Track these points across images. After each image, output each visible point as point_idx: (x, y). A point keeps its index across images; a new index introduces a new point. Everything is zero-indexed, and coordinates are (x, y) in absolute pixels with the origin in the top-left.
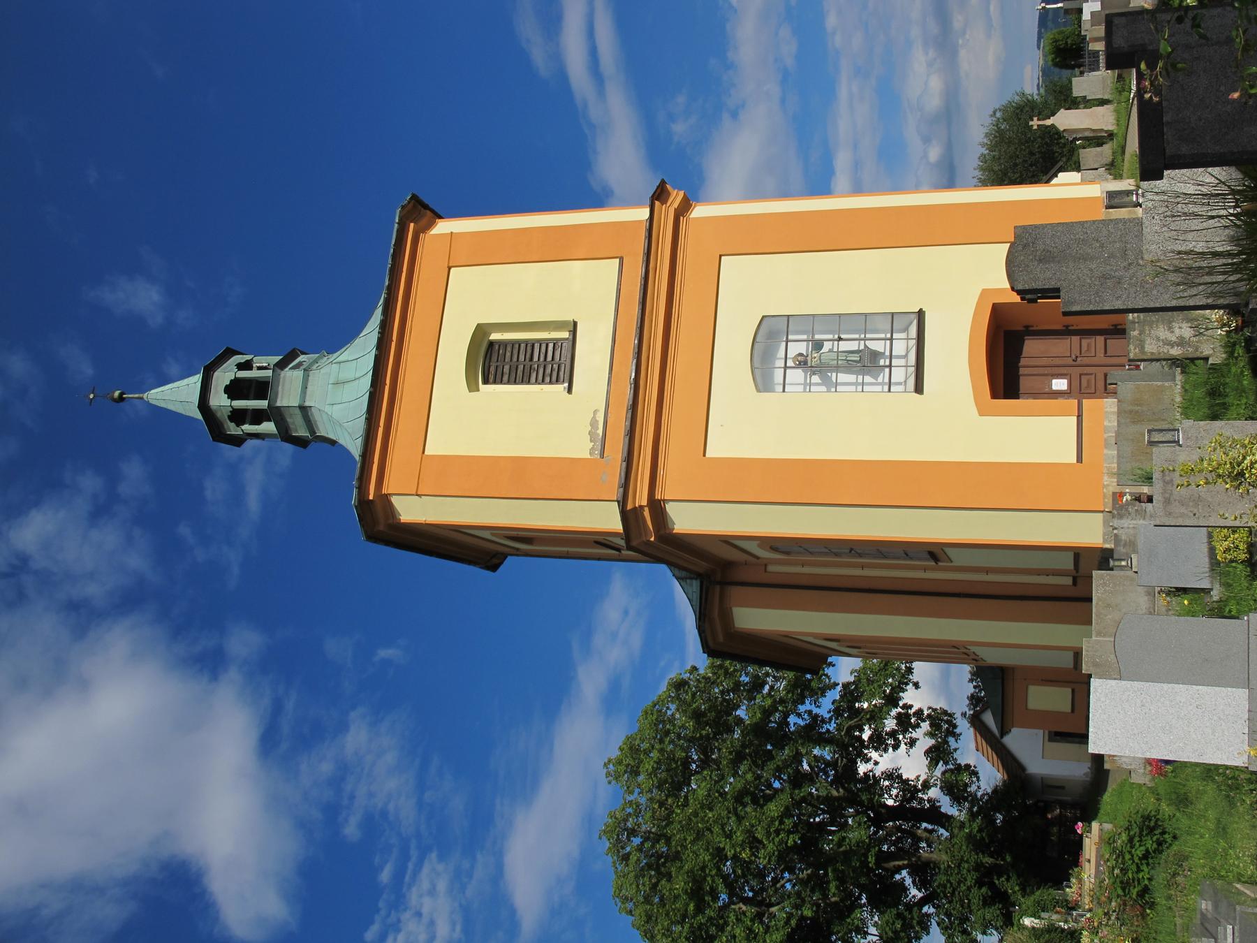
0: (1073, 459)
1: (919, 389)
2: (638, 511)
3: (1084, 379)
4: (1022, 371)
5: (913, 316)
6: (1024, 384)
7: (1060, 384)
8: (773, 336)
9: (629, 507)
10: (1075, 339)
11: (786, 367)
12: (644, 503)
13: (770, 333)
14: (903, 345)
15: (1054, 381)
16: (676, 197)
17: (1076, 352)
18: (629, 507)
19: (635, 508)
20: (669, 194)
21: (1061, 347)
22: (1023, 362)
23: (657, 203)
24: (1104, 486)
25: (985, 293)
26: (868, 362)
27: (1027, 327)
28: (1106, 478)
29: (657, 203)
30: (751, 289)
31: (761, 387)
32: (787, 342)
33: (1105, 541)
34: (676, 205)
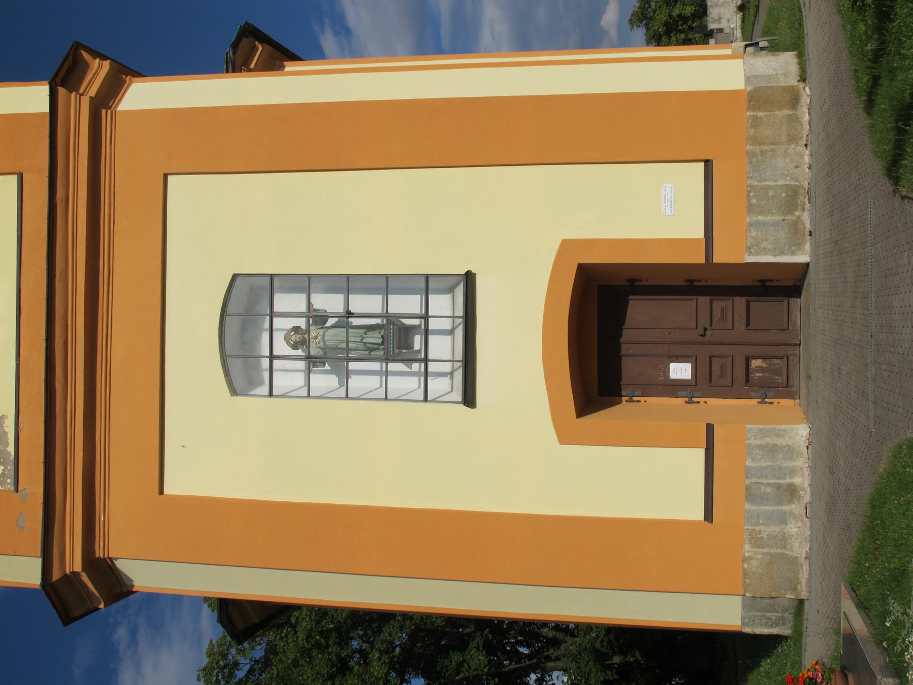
0: (700, 516)
1: (469, 399)
2: (71, 579)
3: (716, 363)
4: (625, 349)
5: (461, 278)
6: (630, 368)
7: (680, 371)
8: (250, 318)
9: (56, 575)
10: (704, 301)
11: (272, 357)
12: (78, 567)
13: (246, 303)
14: (445, 306)
15: (673, 366)
16: (98, 71)
17: (704, 322)
18: (56, 575)
19: (65, 577)
20: (86, 66)
21: (682, 312)
22: (625, 333)
23: (62, 91)
24: (745, 560)
25: (567, 246)
26: (397, 342)
27: (632, 281)
28: (747, 547)
29: (62, 91)
30: (215, 230)
31: (238, 382)
32: (272, 315)
33: (744, 624)
34: (93, 92)
